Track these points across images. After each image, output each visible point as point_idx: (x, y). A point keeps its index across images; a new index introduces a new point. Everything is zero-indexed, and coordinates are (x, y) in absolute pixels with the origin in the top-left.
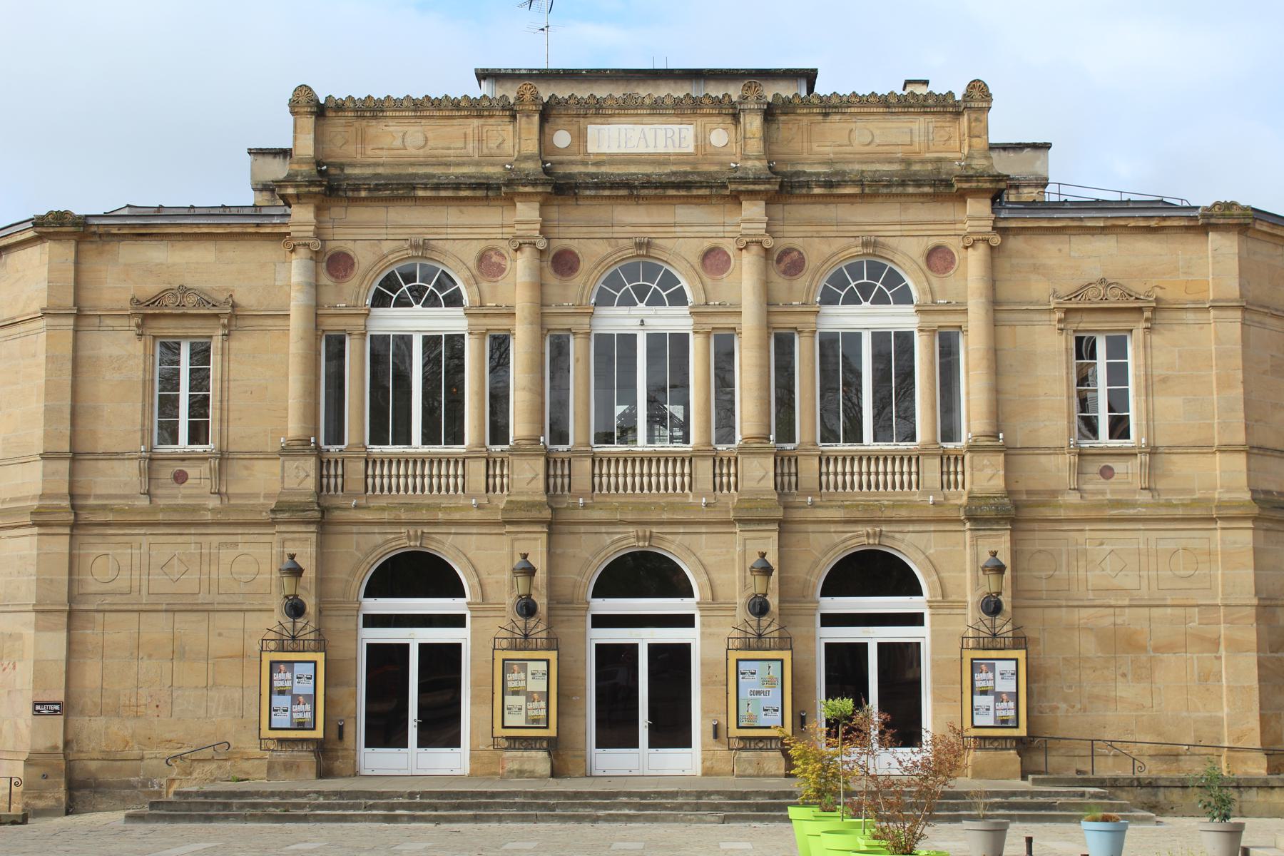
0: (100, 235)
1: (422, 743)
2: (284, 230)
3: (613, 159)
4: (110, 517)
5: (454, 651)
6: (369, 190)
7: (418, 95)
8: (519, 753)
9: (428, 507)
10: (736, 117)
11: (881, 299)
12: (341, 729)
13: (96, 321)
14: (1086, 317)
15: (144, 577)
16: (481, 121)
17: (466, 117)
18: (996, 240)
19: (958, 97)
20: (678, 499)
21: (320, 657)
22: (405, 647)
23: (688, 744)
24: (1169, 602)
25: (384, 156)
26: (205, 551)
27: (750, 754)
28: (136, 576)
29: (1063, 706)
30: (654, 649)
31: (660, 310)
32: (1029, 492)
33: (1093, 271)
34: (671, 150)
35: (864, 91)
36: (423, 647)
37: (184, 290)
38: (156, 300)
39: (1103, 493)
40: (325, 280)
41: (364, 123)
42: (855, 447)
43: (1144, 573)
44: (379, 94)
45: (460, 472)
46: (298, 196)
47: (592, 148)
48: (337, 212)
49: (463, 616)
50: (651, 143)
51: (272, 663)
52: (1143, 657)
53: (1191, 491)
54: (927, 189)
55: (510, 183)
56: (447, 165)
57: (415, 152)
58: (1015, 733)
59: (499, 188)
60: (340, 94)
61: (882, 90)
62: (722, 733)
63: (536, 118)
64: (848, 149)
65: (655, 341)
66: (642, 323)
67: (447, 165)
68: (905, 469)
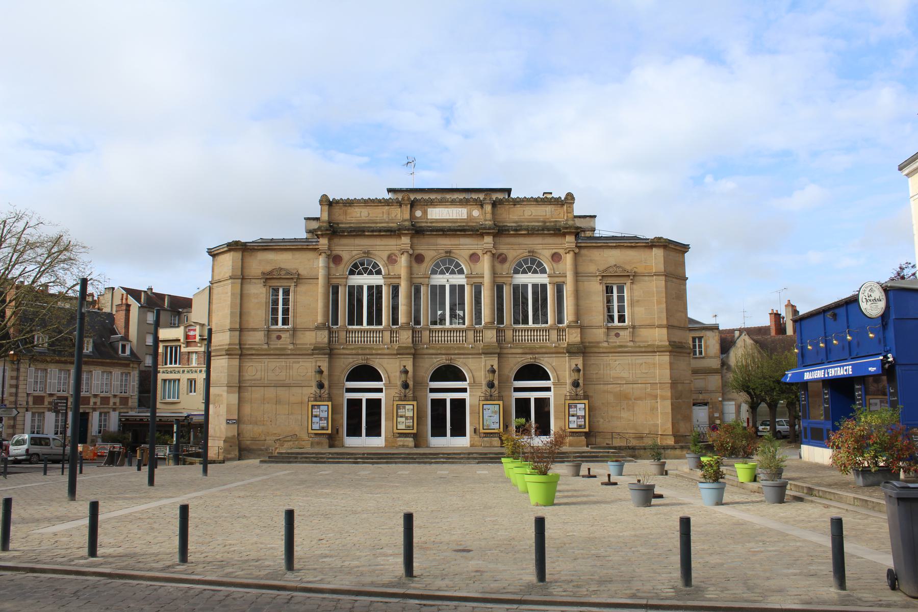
1: (367, 435)
3: (437, 221)
4: (254, 352)
5: (463, 401)
7: (366, 198)
10: (482, 206)
11: (535, 272)
18: (577, 251)
22: (361, 400)
25: (354, 220)
31: (454, 276)
33: (612, 262)
36: (452, 400)
37: (281, 269)
38: (270, 273)
44: (352, 198)
46: (322, 235)
55: (399, 230)
60: (338, 198)
61: (535, 196)
65: (453, 287)
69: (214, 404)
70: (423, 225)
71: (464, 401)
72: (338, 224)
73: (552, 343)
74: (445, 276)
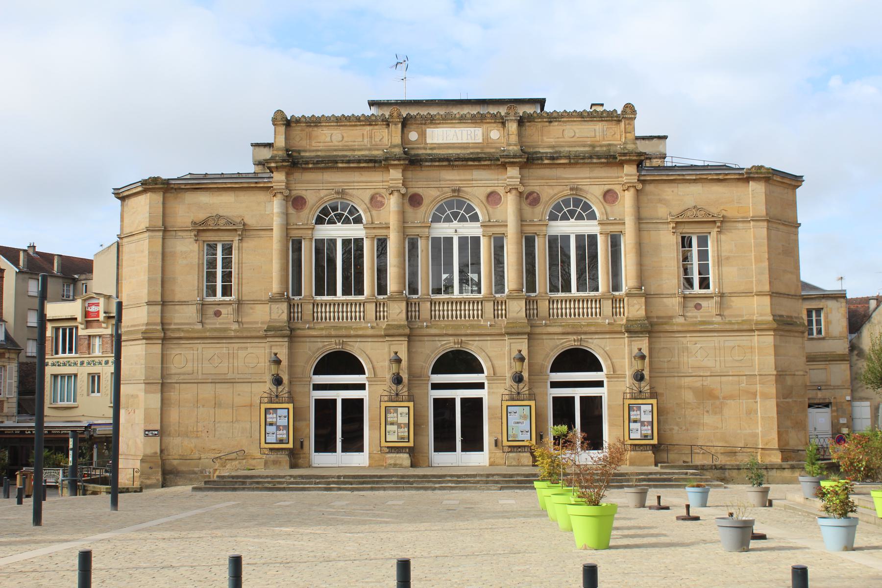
2: (270, 185)
3: (440, 146)
4: (182, 335)
5: (479, 401)
7: (338, 114)
8: (394, 455)
9: (346, 328)
12: (302, 443)
13: (174, 233)
14: (687, 226)
16: (371, 127)
18: (640, 186)
19: (619, 112)
20: (475, 323)
21: (291, 406)
23: (481, 449)
26: (231, 352)
29: (676, 428)
32: (658, 317)
33: (690, 202)
34: (470, 141)
37: (219, 217)
38: (204, 222)
40: (291, 211)
41: (311, 129)
43: (718, 359)
44: (318, 114)
46: (277, 167)
47: (429, 141)
48: (297, 175)
49: (483, 384)
50: (460, 137)
51: (266, 409)
52: (717, 402)
53: (742, 316)
54: (603, 160)
55: (386, 159)
56: (354, 150)
57: (337, 144)
58: (651, 442)
59: (381, 162)
60: (298, 115)
61: (580, 109)
62: (499, 444)
63: (400, 125)
67: (354, 150)
71: (361, 400)
72: (299, 152)
73: (605, 318)
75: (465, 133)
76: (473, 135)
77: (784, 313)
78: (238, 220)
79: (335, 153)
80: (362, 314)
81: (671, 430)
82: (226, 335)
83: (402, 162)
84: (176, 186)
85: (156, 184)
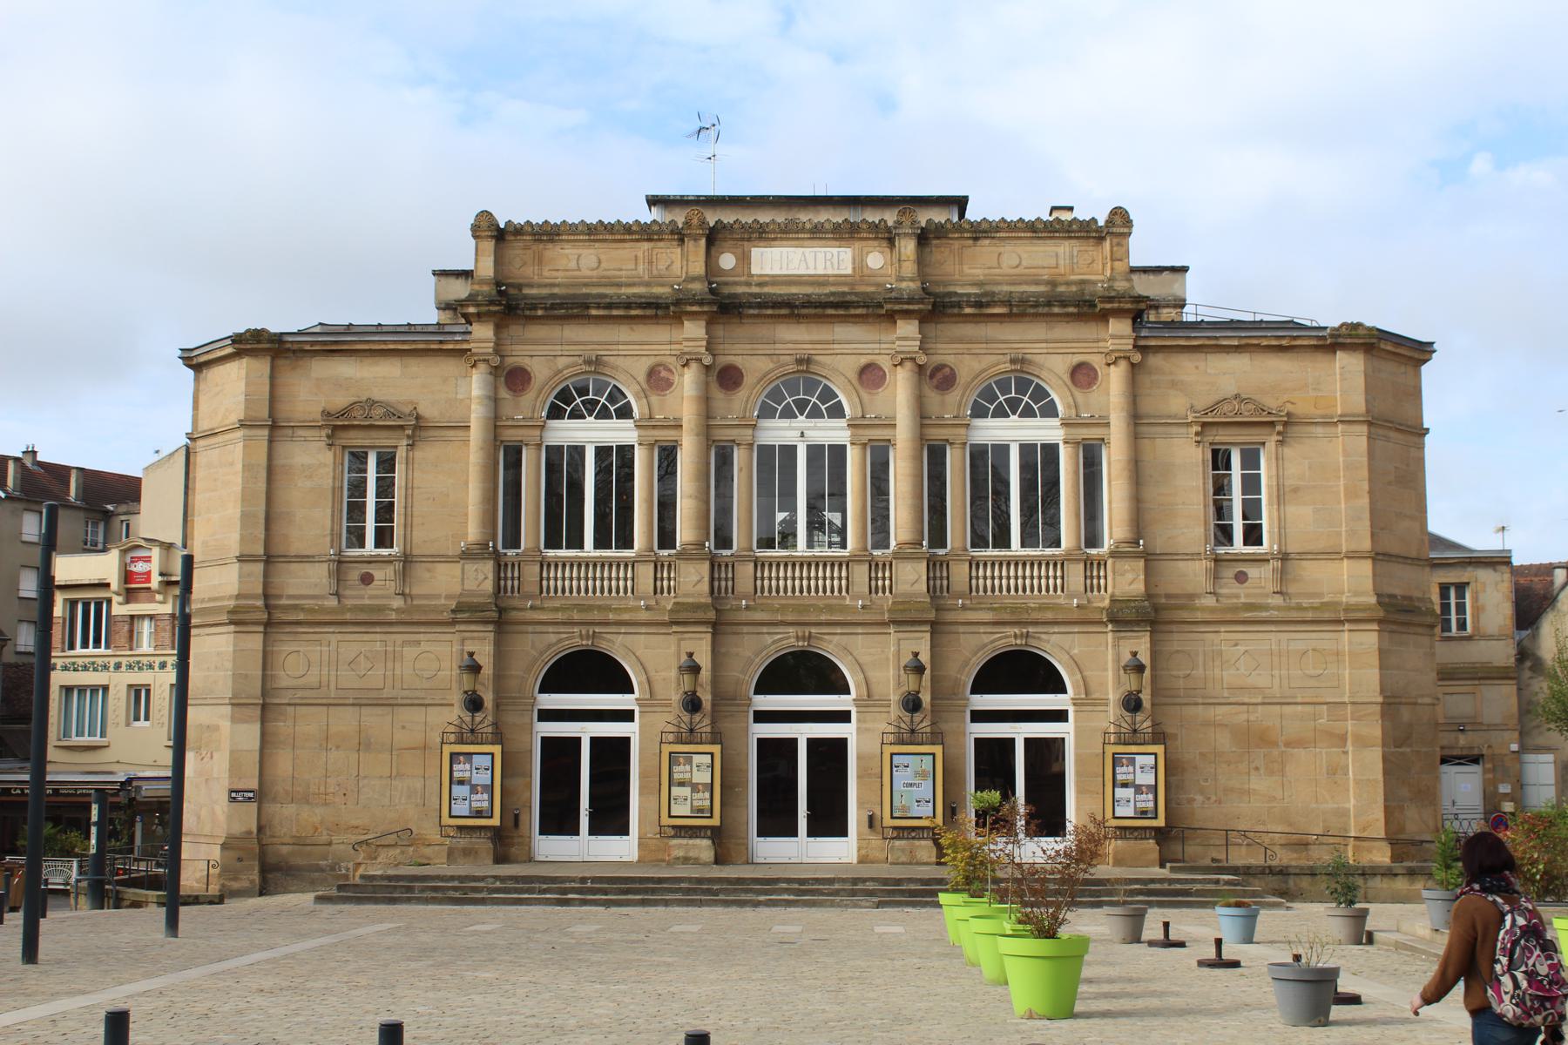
0: (294, 352)
2: (465, 346)
3: (775, 280)
4: (301, 617)
5: (620, 746)
6: (545, 309)
8: (684, 841)
9: (600, 608)
10: (891, 241)
11: (1028, 413)
12: (517, 817)
13: (289, 432)
15: (333, 673)
16: (651, 244)
17: (637, 240)
18: (1137, 358)
19: (1101, 223)
21: (497, 749)
22: (577, 741)
24: (1299, 700)
25: (560, 277)
26: (390, 649)
27: (903, 842)
28: (325, 672)
29: (1199, 798)
30: (813, 743)
32: (1168, 596)
33: (1228, 387)
34: (830, 272)
35: (1012, 216)
37: (372, 403)
38: (344, 413)
39: (1237, 596)
42: (1003, 553)
43: (1276, 672)
44: (555, 219)
45: (844, 574)
46: (479, 315)
48: (515, 330)
50: (811, 264)
51: (452, 755)
52: (1275, 752)
53: (1321, 595)
54: (1071, 310)
55: (678, 303)
56: (619, 285)
57: (589, 273)
58: (1154, 823)
60: (519, 220)
61: (1029, 216)
62: (877, 823)
63: (703, 242)
64: (997, 271)
66: (802, 435)
67: (619, 285)
68: (1051, 573)
69: (198, 749)
70: (740, 290)
71: (625, 741)
73: (1071, 597)
74: (794, 423)
75: (821, 256)
76: (835, 260)
77: (1397, 592)
78: (407, 410)
79: (584, 290)
80: (629, 583)
81: (1191, 801)
82: (381, 618)
83: (706, 309)
84: (296, 347)
85: (259, 342)
